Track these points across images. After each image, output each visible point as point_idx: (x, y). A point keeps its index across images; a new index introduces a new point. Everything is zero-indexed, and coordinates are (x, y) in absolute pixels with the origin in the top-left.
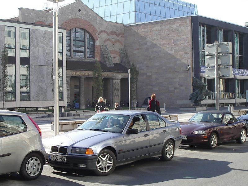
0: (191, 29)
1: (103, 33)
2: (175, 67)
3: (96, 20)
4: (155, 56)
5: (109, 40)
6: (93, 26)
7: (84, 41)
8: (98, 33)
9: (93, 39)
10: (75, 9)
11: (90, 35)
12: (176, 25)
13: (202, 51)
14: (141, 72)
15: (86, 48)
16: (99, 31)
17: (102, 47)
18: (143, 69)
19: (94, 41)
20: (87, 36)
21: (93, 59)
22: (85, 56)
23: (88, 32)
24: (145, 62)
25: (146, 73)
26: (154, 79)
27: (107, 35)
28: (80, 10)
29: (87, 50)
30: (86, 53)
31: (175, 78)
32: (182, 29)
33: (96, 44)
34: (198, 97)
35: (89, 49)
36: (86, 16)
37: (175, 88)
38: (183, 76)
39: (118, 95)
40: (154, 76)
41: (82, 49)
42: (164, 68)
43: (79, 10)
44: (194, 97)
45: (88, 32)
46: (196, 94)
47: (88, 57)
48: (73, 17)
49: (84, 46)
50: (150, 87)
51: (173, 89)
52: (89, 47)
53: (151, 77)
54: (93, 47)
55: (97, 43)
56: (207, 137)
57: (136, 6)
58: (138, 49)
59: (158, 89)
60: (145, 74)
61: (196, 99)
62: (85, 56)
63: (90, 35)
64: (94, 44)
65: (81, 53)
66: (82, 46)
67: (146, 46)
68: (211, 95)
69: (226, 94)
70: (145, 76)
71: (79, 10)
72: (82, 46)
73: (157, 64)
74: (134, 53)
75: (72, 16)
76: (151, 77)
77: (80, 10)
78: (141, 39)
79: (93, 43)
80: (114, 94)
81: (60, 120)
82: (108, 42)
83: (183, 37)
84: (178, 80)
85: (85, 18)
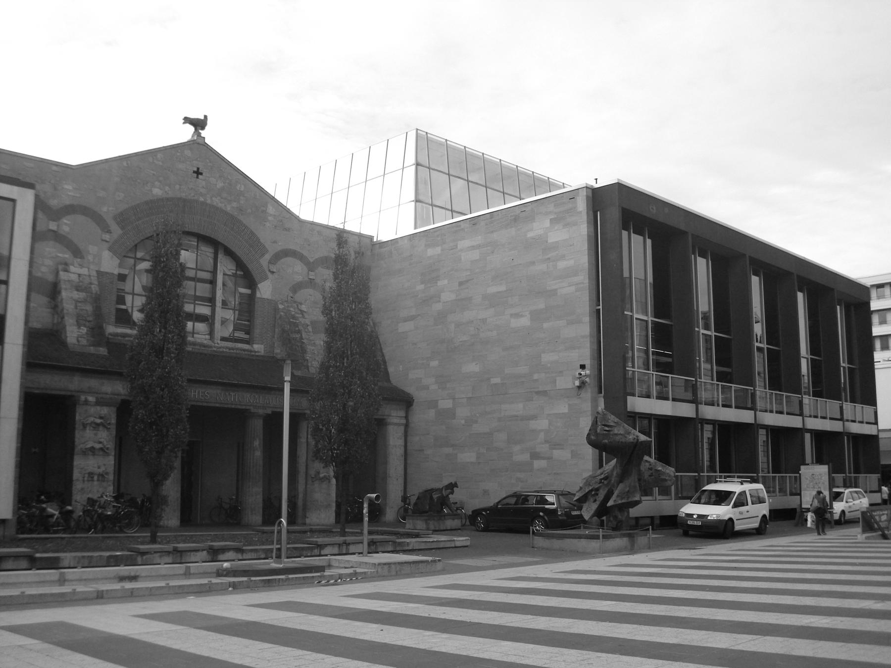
0: (593, 234)
1: (289, 260)
2: (536, 377)
3: (264, 212)
4: (465, 338)
5: (311, 283)
6: (252, 233)
7: (213, 282)
8: (267, 257)
9: (247, 276)
10: (181, 166)
11: (240, 264)
12: (539, 227)
13: (635, 316)
14: (419, 396)
15: (219, 304)
16: (272, 249)
17: (281, 307)
18: (427, 388)
19: (251, 283)
20: (226, 266)
21: (246, 346)
22: (211, 333)
23: (229, 253)
24: (434, 363)
25: (437, 401)
26: (463, 422)
27: (305, 268)
28: (201, 174)
29: (220, 313)
30: (217, 325)
31: (534, 417)
32: (557, 235)
33: (258, 295)
34: (616, 493)
35: (234, 310)
36: (224, 195)
37: (535, 456)
38: (562, 408)
39: (327, 479)
40: (462, 413)
41: (204, 310)
42: (496, 380)
43: (198, 173)
44: (597, 490)
45: (229, 253)
46: (606, 478)
47: (223, 339)
48: (171, 194)
49: (211, 300)
50: (448, 450)
51: (526, 457)
52: (233, 302)
53: (450, 414)
54: (248, 308)
55: (265, 290)
56: (626, 274)
57: (421, 186)
58: (412, 318)
59: (473, 460)
60: (433, 404)
61: (607, 498)
62: (211, 333)
63: (240, 264)
64: (252, 298)
65: (196, 324)
66: (202, 299)
67: (438, 307)
68: (669, 483)
69: (774, 478)
70: (432, 413)
71: (198, 173)
72: (202, 299)
73: (473, 368)
74: (400, 331)
75: (167, 188)
76: (450, 414)
77: (201, 174)
78: (422, 283)
79: (248, 291)
80: (312, 473)
81: (370, 533)
82: (310, 291)
83: (562, 265)
84: (542, 424)
85: (216, 201)
